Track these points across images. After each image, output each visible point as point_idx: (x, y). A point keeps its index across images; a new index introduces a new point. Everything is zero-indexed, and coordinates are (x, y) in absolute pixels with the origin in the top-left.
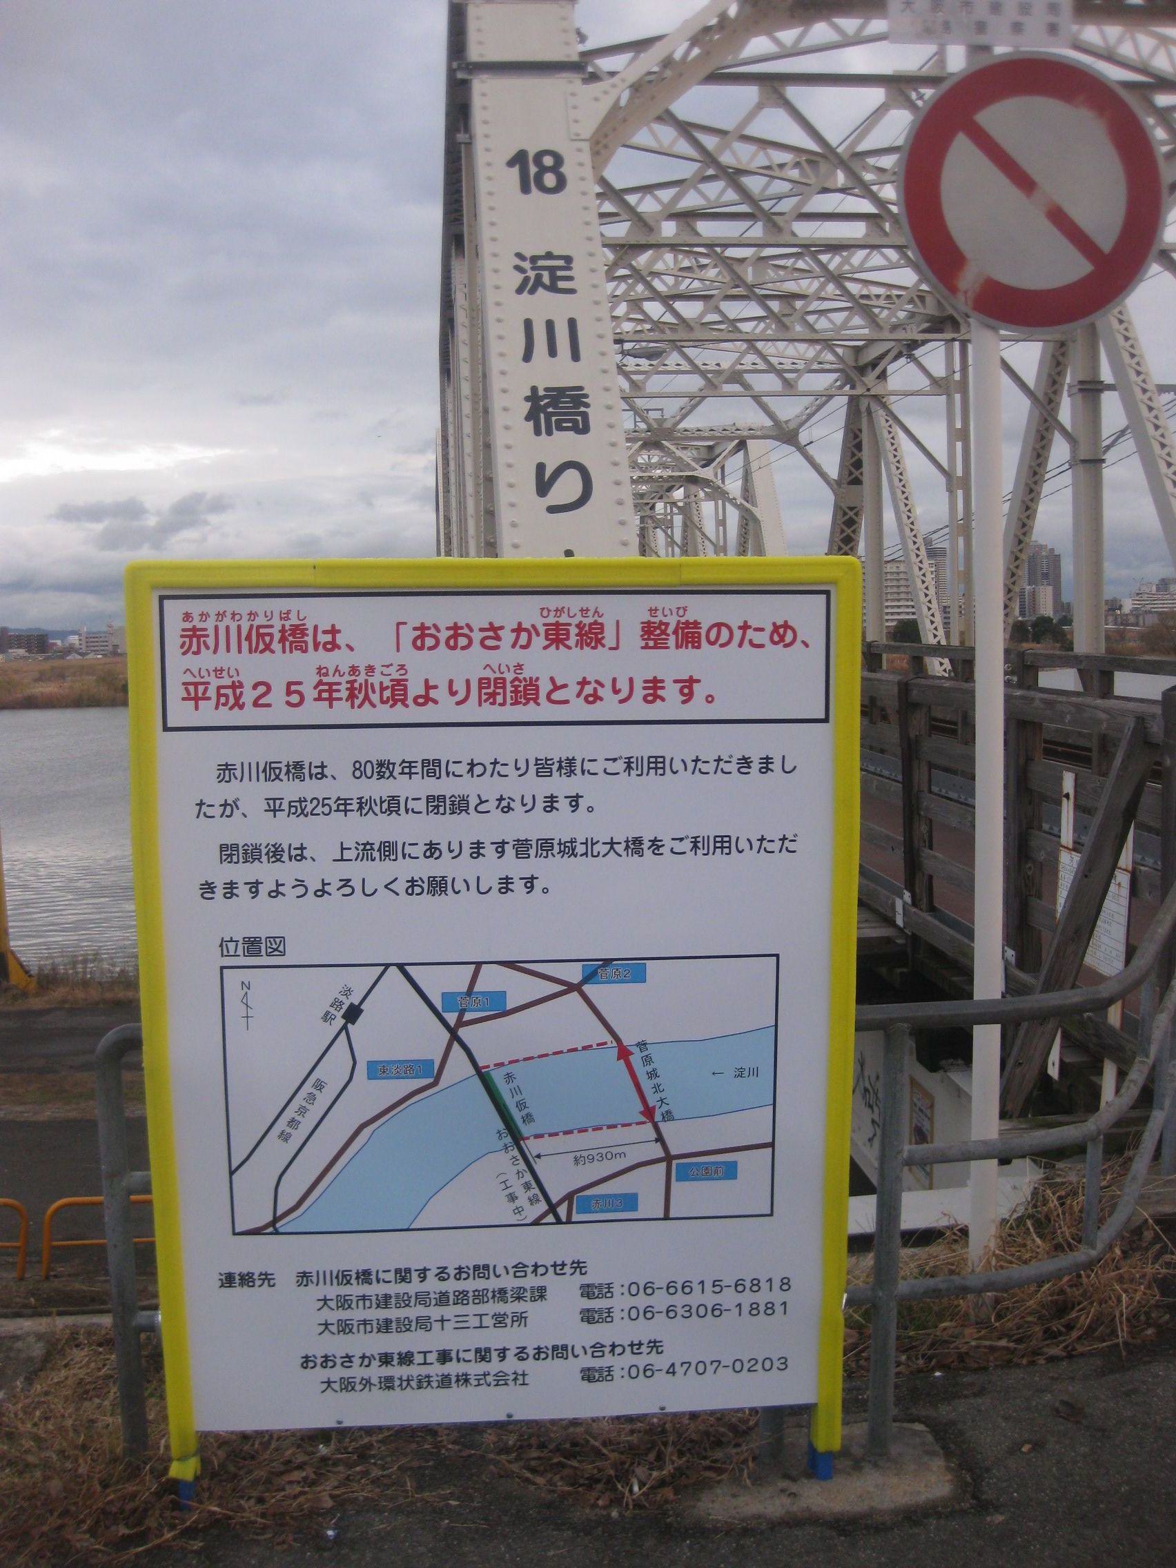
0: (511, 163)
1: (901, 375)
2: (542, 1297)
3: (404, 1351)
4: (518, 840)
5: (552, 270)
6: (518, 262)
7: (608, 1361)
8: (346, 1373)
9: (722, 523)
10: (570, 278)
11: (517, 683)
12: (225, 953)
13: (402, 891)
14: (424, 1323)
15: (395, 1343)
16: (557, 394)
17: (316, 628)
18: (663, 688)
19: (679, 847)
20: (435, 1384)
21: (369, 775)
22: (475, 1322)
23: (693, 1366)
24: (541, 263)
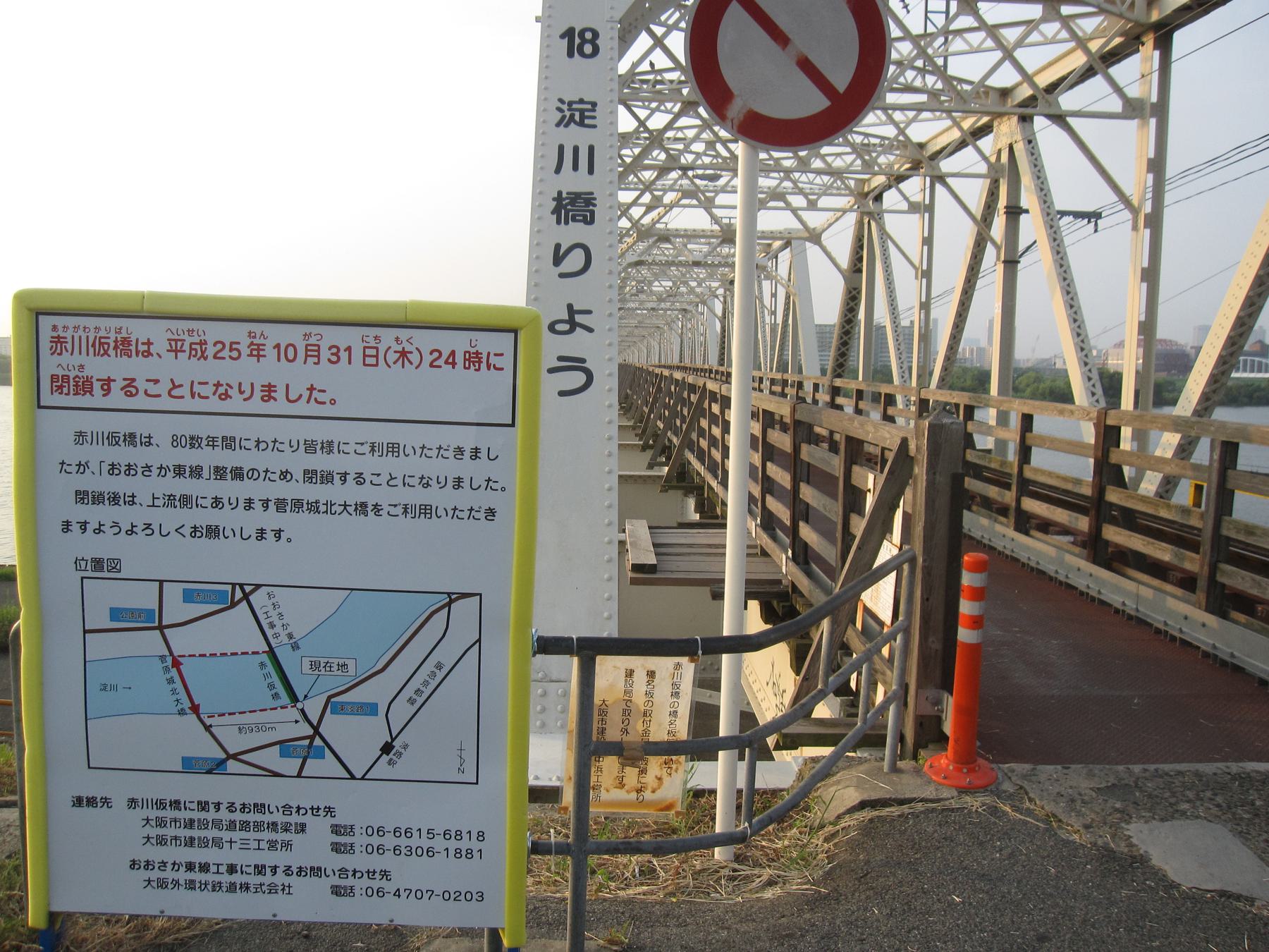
0: (562, 36)
1: (891, 198)
2: (303, 831)
3: (203, 862)
4: (278, 499)
5: (582, 112)
6: (560, 105)
7: (350, 882)
8: (162, 875)
9: (774, 295)
10: (594, 118)
11: (77, 379)
12: (78, 568)
13: (188, 535)
14: (218, 843)
15: (197, 855)
16: (574, 197)
17: (137, 340)
18: (275, 391)
19: (393, 511)
20: (224, 889)
21: (183, 445)
22: (255, 845)
23: (413, 892)
24: (574, 106)
